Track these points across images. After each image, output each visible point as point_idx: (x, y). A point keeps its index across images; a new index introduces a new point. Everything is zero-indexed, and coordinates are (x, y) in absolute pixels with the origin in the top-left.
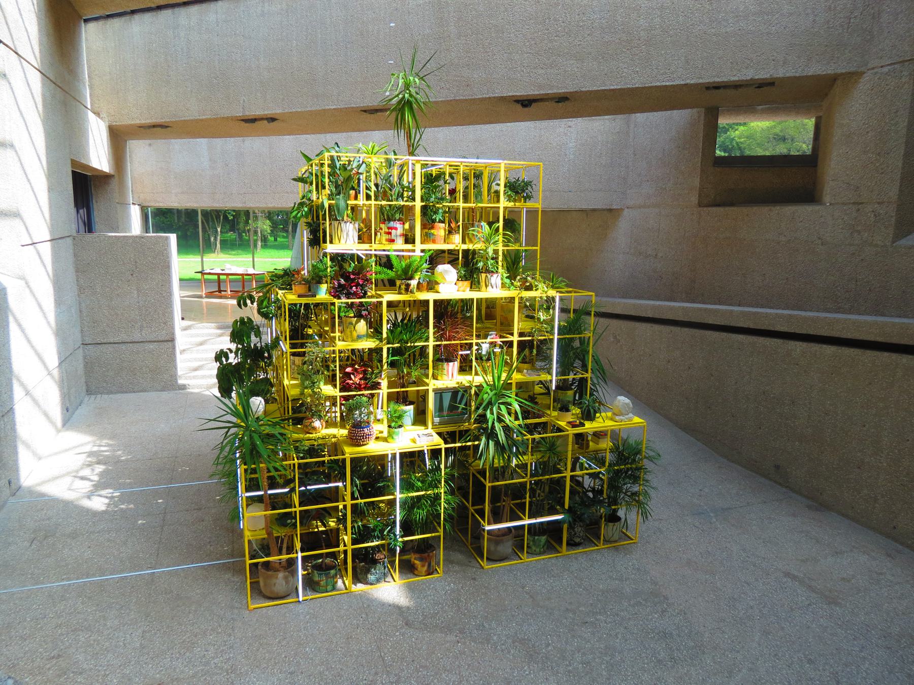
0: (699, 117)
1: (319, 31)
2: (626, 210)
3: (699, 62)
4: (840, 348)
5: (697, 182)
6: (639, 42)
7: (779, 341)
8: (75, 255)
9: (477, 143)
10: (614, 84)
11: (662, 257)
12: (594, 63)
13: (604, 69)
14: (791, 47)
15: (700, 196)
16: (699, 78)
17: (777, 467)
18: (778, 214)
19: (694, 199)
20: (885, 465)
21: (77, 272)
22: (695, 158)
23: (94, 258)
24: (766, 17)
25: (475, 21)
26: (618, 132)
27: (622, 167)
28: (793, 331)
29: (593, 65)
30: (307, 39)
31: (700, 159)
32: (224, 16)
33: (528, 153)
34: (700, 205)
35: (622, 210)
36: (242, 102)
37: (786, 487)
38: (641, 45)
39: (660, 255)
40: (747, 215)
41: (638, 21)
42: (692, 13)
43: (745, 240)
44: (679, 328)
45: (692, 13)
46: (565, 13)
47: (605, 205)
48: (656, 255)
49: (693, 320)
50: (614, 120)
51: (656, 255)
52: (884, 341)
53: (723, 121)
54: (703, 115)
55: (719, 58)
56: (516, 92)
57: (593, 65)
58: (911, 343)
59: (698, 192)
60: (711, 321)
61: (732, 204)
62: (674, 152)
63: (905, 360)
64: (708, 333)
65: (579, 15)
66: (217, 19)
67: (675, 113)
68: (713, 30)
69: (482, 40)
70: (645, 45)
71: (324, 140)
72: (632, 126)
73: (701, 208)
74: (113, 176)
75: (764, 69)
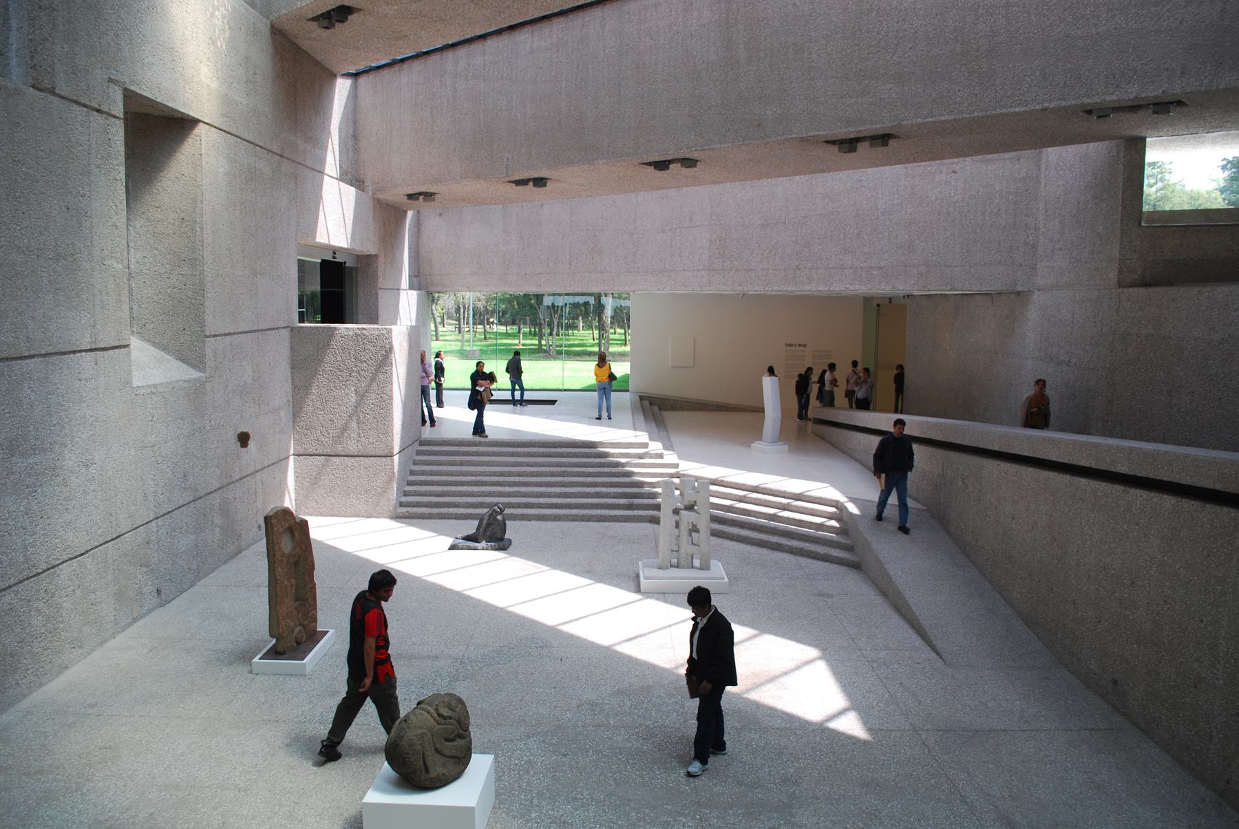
0: (1118, 153)
1: (590, 67)
2: (1037, 293)
3: (1060, 76)
4: (1180, 499)
5: (1116, 251)
6: (977, 54)
7: (1118, 488)
8: (292, 349)
9: (827, 200)
10: (945, 113)
11: (1075, 364)
12: (919, 86)
13: (931, 94)
14: (1191, 49)
15: (1120, 271)
16: (1062, 99)
17: (1115, 682)
18: (1209, 298)
19: (1113, 275)
20: (1221, 682)
21: (292, 368)
22: (1113, 214)
23: (312, 353)
24: (1153, 9)
25: (769, 40)
26: (1024, 178)
27: (1030, 229)
28: (1133, 473)
29: (917, 88)
30: (577, 78)
31: (1120, 215)
32: (491, 57)
33: (895, 211)
34: (1120, 284)
35: (1030, 292)
36: (505, 160)
37: (1124, 714)
38: (980, 58)
39: (1073, 361)
40: (1173, 300)
41: (975, 24)
42: (1048, 10)
43: (1171, 338)
44: (1024, 468)
45: (1048, 10)
46: (880, 21)
47: (1006, 285)
48: (1069, 361)
49: (1038, 456)
50: (1018, 160)
51: (1069, 361)
52: (1222, 489)
53: (1151, 155)
54: (1123, 149)
55: (1088, 70)
56: (818, 131)
57: (917, 88)
58: (1233, 488)
59: (1117, 265)
60: (1053, 457)
61: (1170, 283)
62: (1090, 206)
63: (3, 356)
64: (1052, 475)
65: (898, 23)
66: (485, 62)
67: (1092, 146)
68: (1079, 32)
69: (777, 64)
70: (986, 56)
71: (634, 202)
72: (1043, 167)
73: (1121, 290)
74: (376, 256)
75: (1153, 82)
